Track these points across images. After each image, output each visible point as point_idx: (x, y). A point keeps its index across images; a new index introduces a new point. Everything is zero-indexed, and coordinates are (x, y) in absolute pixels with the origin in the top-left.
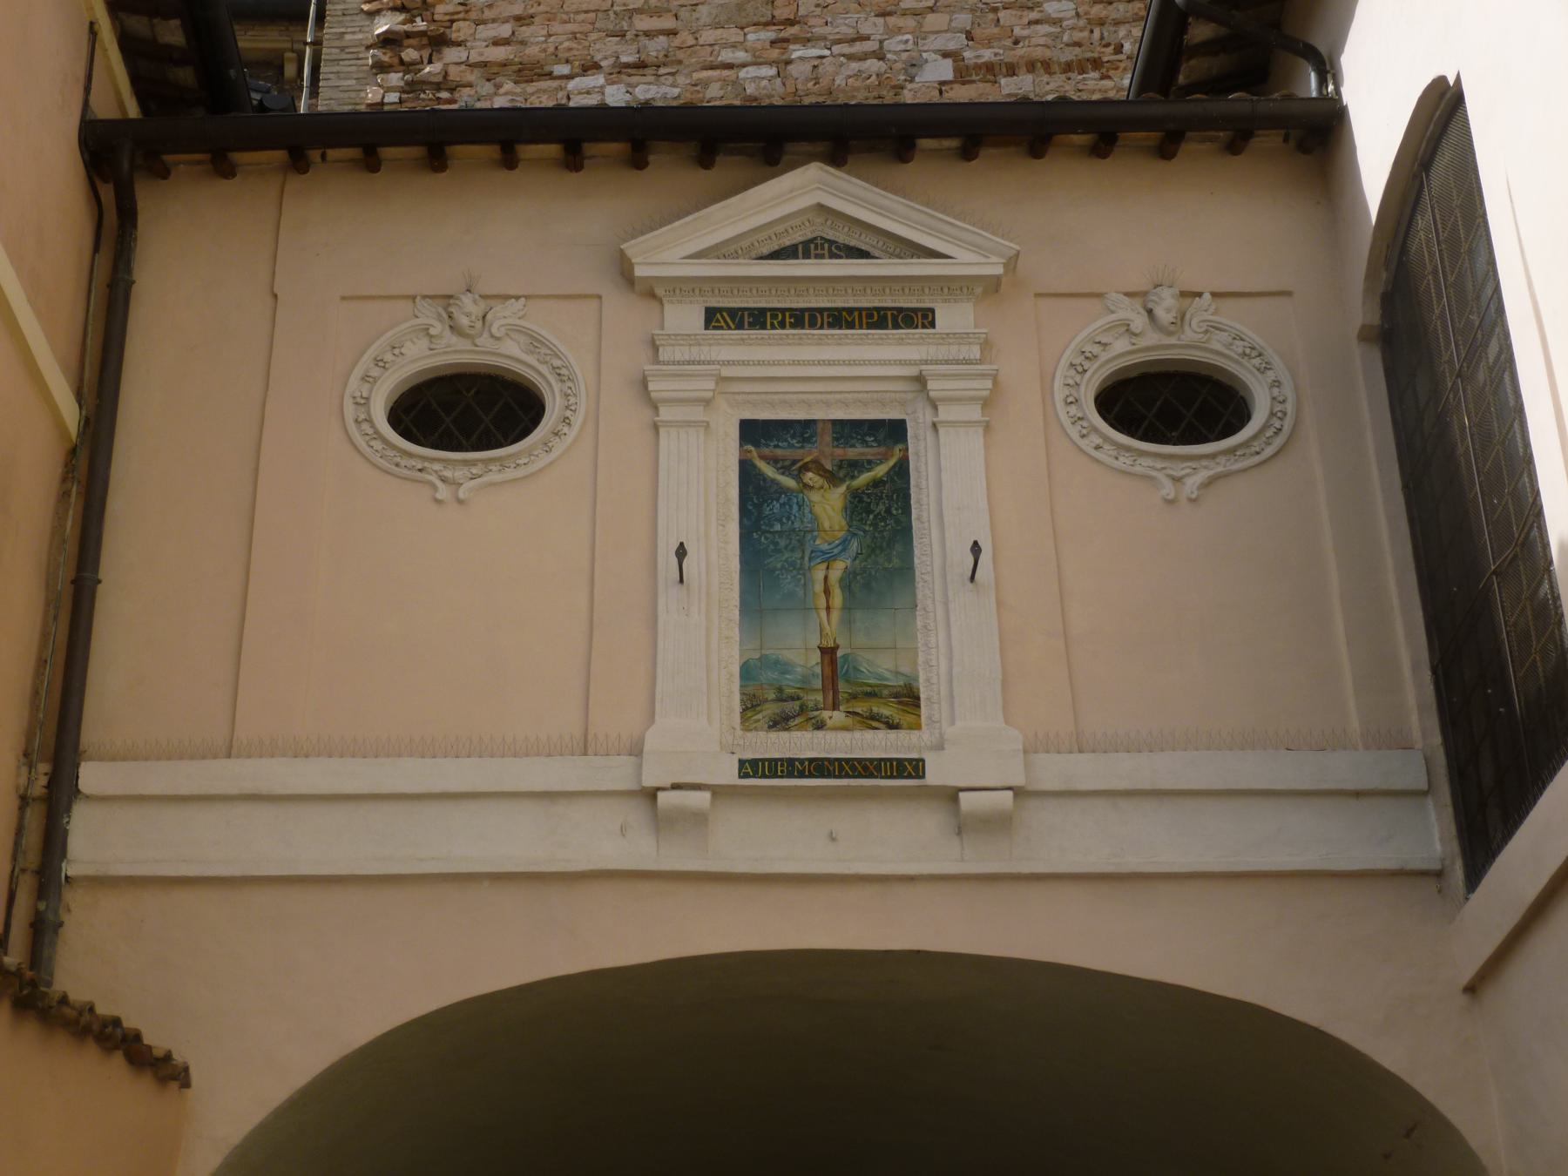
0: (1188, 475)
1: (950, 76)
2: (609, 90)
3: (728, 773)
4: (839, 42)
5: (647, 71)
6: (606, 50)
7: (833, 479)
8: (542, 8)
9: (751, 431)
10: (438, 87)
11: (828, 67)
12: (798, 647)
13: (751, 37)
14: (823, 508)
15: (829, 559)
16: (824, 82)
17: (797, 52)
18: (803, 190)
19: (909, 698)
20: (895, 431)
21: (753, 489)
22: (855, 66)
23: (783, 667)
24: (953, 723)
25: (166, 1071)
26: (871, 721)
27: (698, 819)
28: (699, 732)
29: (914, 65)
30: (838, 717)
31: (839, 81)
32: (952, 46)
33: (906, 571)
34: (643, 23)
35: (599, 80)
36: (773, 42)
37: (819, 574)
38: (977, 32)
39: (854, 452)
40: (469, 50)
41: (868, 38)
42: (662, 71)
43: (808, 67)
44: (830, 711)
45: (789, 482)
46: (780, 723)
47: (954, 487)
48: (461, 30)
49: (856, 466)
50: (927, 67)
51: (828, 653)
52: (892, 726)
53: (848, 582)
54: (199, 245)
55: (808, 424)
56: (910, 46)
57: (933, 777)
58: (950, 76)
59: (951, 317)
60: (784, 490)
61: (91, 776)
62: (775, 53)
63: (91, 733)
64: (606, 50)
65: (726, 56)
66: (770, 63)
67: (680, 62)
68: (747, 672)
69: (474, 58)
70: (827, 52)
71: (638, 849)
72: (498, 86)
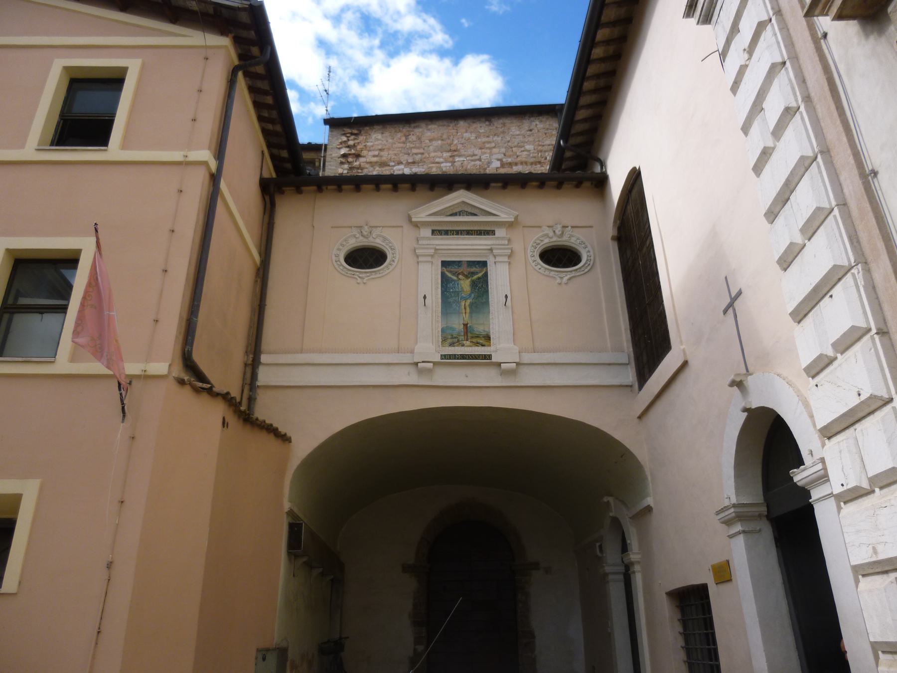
3: (438, 359)
6: (404, 158)
7: (467, 277)
9: (445, 264)
12: (457, 324)
14: (467, 284)
15: (466, 299)
17: (457, 159)
18: (460, 196)
19: (488, 338)
20: (484, 264)
23: (453, 329)
25: (285, 439)
26: (477, 344)
28: (429, 347)
33: (487, 303)
34: (415, 151)
35: (402, 167)
37: (463, 304)
39: (473, 269)
44: (467, 340)
45: (455, 278)
48: (364, 153)
49: (473, 274)
51: (465, 325)
52: (483, 345)
53: (471, 305)
54: (293, 215)
55: (460, 262)
57: (494, 360)
59: (500, 232)
60: (453, 280)
62: (451, 159)
63: (264, 346)
68: (443, 331)
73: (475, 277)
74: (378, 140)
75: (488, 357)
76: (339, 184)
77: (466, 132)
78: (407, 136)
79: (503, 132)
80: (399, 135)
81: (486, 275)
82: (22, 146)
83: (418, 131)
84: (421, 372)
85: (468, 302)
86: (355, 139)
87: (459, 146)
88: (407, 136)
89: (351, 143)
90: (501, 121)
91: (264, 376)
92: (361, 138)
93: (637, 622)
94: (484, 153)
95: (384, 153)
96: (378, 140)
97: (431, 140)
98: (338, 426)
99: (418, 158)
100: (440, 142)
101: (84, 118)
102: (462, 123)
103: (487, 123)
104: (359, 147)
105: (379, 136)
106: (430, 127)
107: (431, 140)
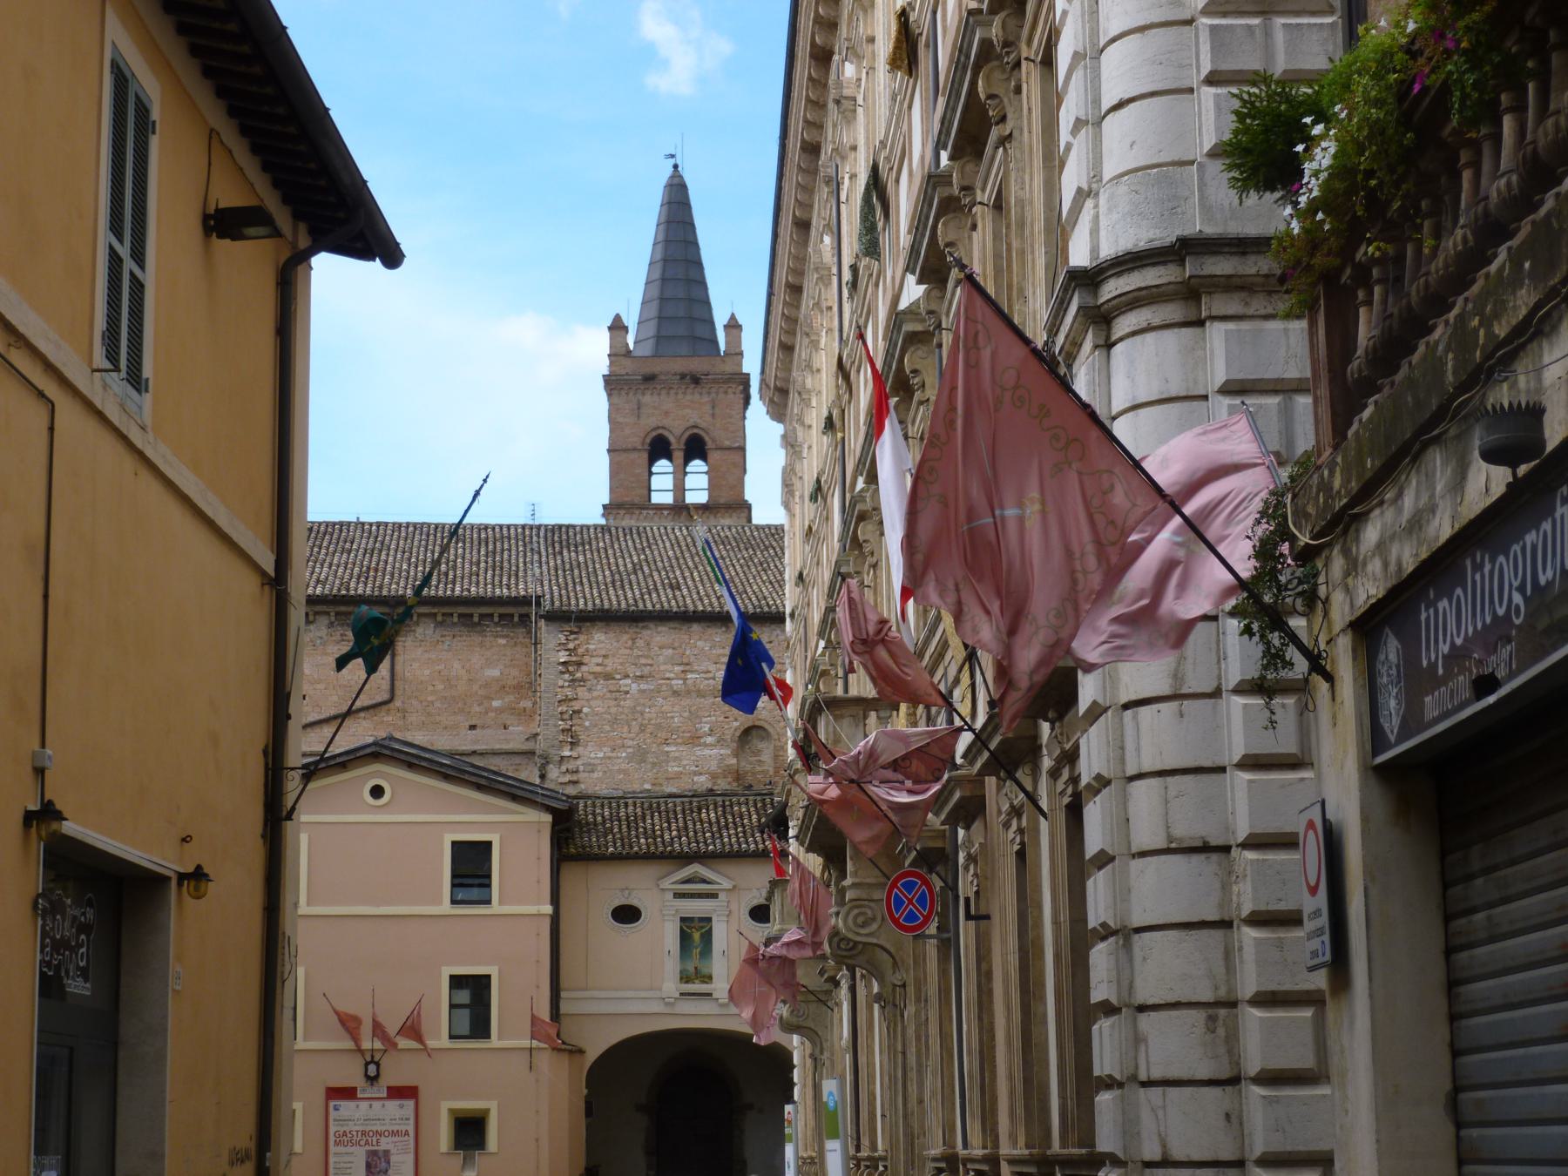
0: (849, 592)
6: (631, 670)
9: (683, 919)
12: (690, 968)
14: (695, 936)
17: (690, 676)
18: (696, 869)
19: (710, 977)
25: (581, 1052)
28: (671, 986)
33: (710, 951)
34: (643, 661)
35: (628, 681)
47: (721, 934)
48: (586, 659)
54: (573, 876)
59: (722, 896)
61: (563, 994)
63: (562, 985)
64: (631, 670)
74: (600, 642)
78: (633, 640)
80: (625, 637)
82: (440, 903)
83: (646, 633)
84: (667, 1004)
87: (692, 659)
88: (633, 640)
89: (571, 646)
91: (565, 1008)
92: (582, 638)
95: (608, 662)
96: (600, 642)
97: (661, 648)
98: (614, 1041)
99: (647, 670)
101: (471, 868)
102: (695, 627)
104: (580, 651)
107: (661, 648)
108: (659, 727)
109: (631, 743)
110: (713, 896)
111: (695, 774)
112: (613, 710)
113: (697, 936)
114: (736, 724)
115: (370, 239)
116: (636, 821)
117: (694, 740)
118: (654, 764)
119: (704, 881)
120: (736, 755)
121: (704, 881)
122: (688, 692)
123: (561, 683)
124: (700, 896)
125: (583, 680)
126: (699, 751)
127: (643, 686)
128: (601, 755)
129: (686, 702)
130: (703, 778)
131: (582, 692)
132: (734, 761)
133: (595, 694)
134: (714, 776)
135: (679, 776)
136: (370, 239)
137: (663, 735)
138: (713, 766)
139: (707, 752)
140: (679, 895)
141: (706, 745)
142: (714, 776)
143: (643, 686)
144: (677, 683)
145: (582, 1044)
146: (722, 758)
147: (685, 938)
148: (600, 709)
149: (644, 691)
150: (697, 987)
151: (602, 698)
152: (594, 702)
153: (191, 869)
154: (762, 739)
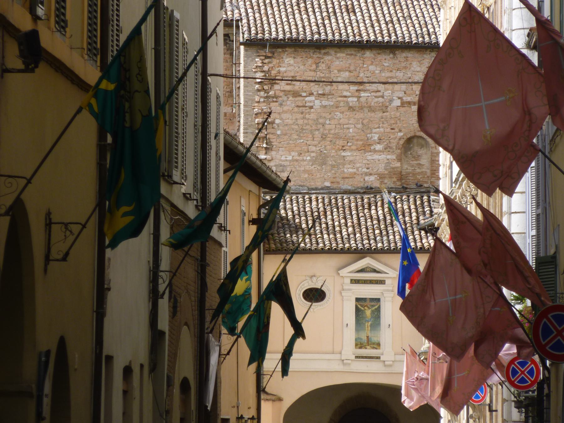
1: (399, 104)
2: (316, 101)
3: (353, 357)
4: (373, 92)
5: (325, 96)
7: (369, 308)
8: (298, 74)
9: (358, 300)
10: (273, 97)
11: (370, 100)
13: (351, 88)
15: (368, 322)
16: (369, 104)
17: (363, 94)
18: (367, 261)
19: (379, 344)
20: (378, 300)
21: (357, 310)
22: (376, 100)
23: (361, 339)
24: (380, 91)
25: (280, 399)
26: (374, 348)
27: (349, 364)
28: (349, 350)
29: (391, 101)
30: (368, 347)
31: (372, 104)
32: (401, 96)
33: (379, 324)
35: (312, 98)
36: (357, 90)
37: (367, 324)
38: (407, 92)
39: (373, 304)
40: (280, 86)
41: (380, 91)
42: (329, 97)
43: (365, 99)
44: (366, 344)
45: (362, 309)
46: (360, 348)
49: (373, 306)
50: (394, 101)
51: (368, 337)
52: (376, 349)
53: (371, 325)
55: (366, 299)
56: (390, 94)
57: (382, 359)
58: (399, 104)
60: (361, 310)
62: (357, 94)
65: (345, 93)
66: (356, 97)
67: (333, 94)
68: (356, 340)
69: (282, 89)
70: (370, 95)
71: (340, 368)
72: (288, 98)
73: (374, 308)
74: (290, 65)
75: (378, 358)
76: (309, 252)
77: (372, 64)
78: (317, 64)
79: (405, 68)
80: (310, 61)
81: (379, 307)
83: (327, 58)
84: (344, 364)
85: (370, 323)
86: (269, 63)
88: (317, 64)
89: (266, 68)
90: (404, 55)
92: (275, 61)
93: (219, 404)
94: (386, 90)
96: (290, 65)
97: (339, 71)
100: (347, 74)
102: (368, 54)
103: (391, 56)
105: (292, 61)
106: (338, 55)
107: (339, 71)
108: (337, 136)
109: (314, 149)
110: (382, 282)
111: (366, 174)
112: (300, 122)
113: (368, 312)
114: (400, 134)
115: (304, 337)
116: (319, 217)
117: (366, 147)
118: (333, 166)
119: (375, 271)
120: (399, 159)
121: (375, 271)
122: (362, 108)
123: (257, 99)
124: (371, 282)
125: (275, 96)
126: (369, 156)
127: (325, 103)
128: (290, 158)
129: (359, 115)
130: (372, 178)
131: (275, 107)
132: (398, 164)
133: (285, 108)
134: (381, 177)
135: (352, 176)
136: (304, 337)
137: (341, 143)
138: (381, 168)
139: (376, 157)
140: (355, 281)
141: (375, 151)
142: (381, 177)
143: (325, 103)
144: (352, 101)
145: (282, 396)
146: (388, 162)
147: (358, 312)
148: (290, 122)
149: (325, 107)
150: (368, 351)
151: (291, 112)
152: (285, 115)
153: (251, 417)
154: (422, 146)
